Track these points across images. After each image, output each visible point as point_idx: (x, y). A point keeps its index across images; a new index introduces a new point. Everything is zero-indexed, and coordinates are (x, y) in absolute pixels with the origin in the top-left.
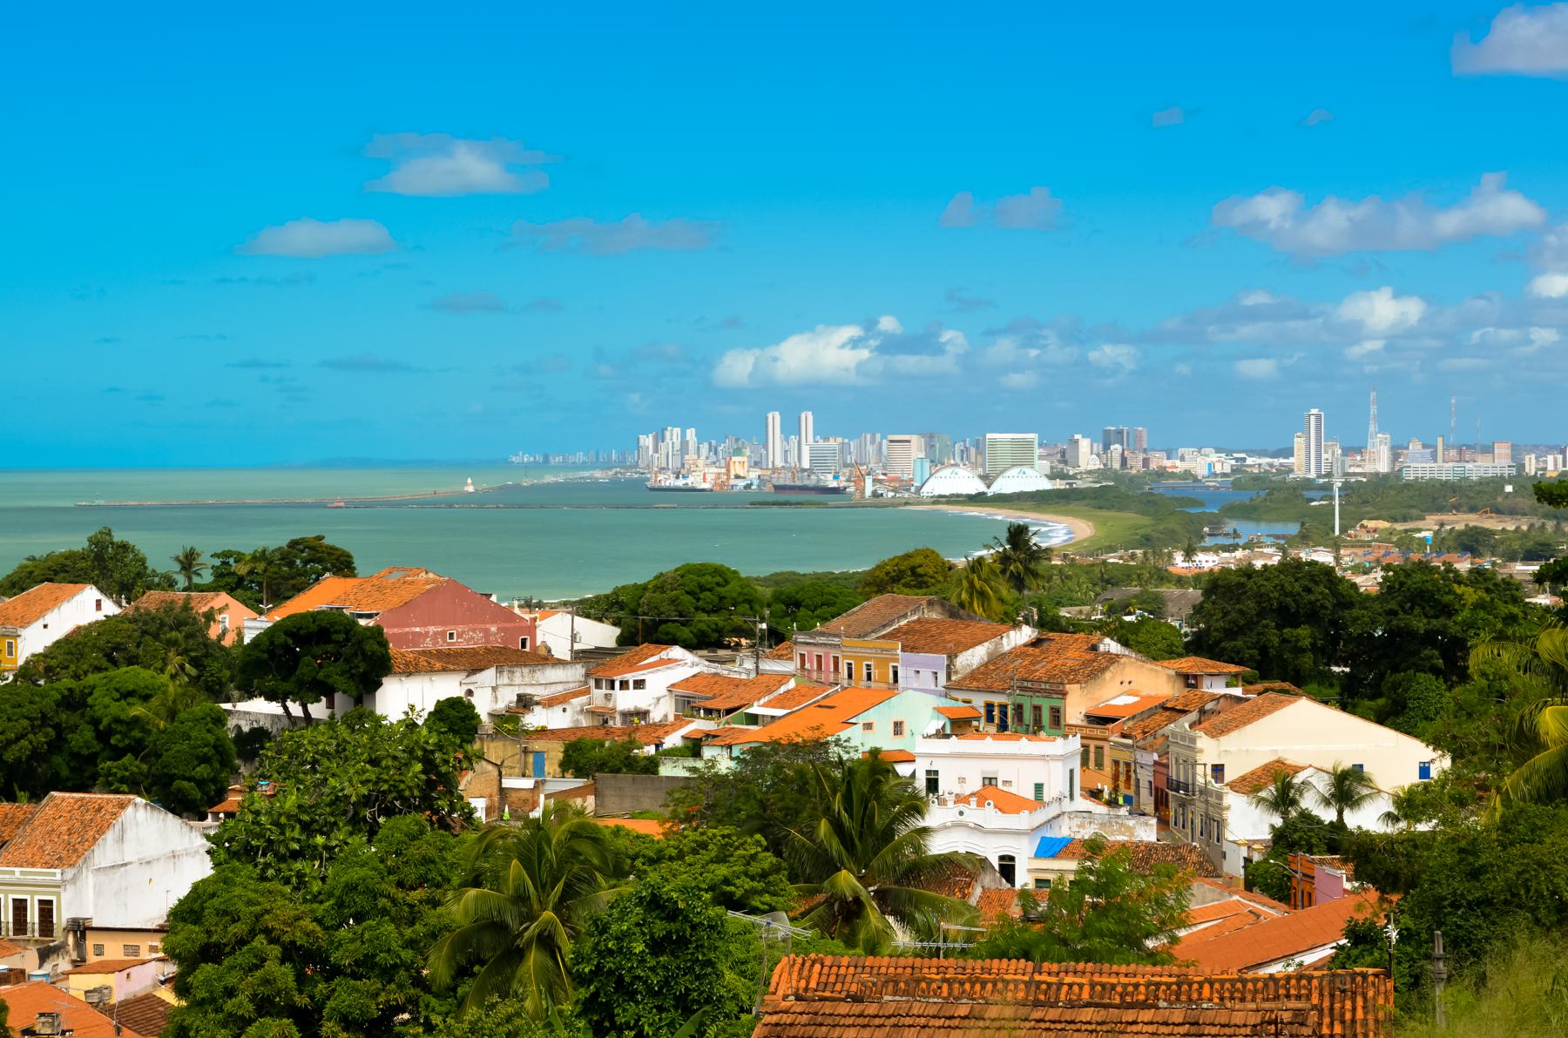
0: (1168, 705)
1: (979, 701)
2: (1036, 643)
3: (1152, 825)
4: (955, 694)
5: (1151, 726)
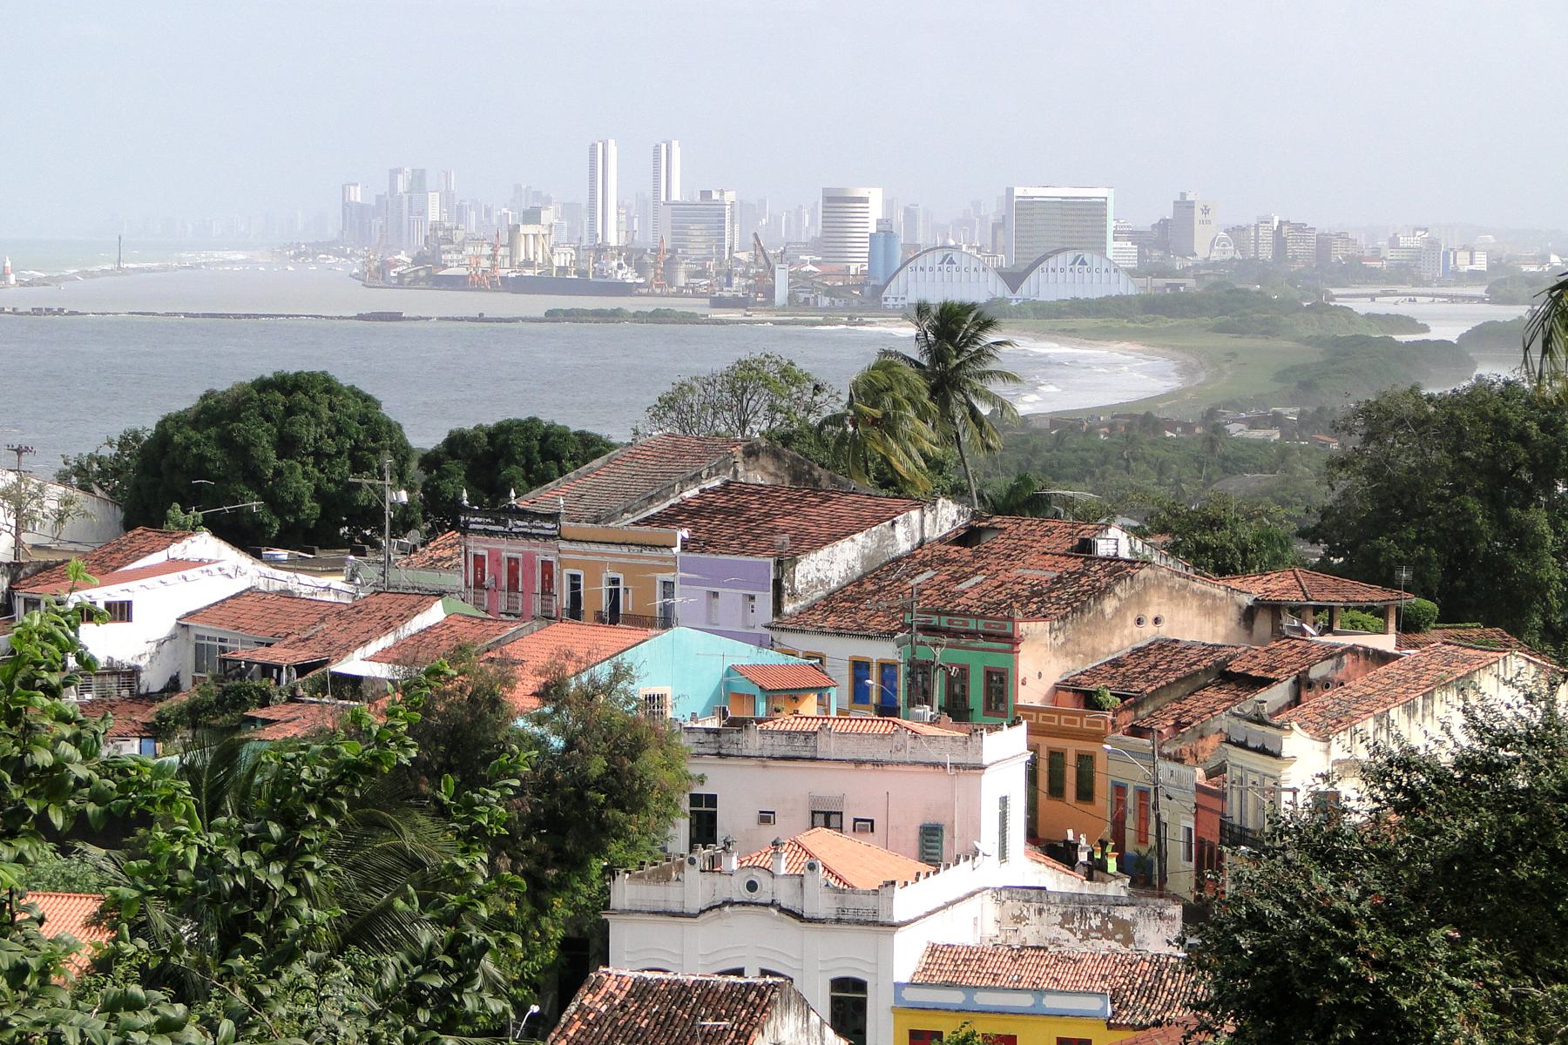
0: (1236, 667)
1: (841, 652)
2: (968, 537)
3: (1172, 918)
4: (790, 640)
5: (1196, 712)
